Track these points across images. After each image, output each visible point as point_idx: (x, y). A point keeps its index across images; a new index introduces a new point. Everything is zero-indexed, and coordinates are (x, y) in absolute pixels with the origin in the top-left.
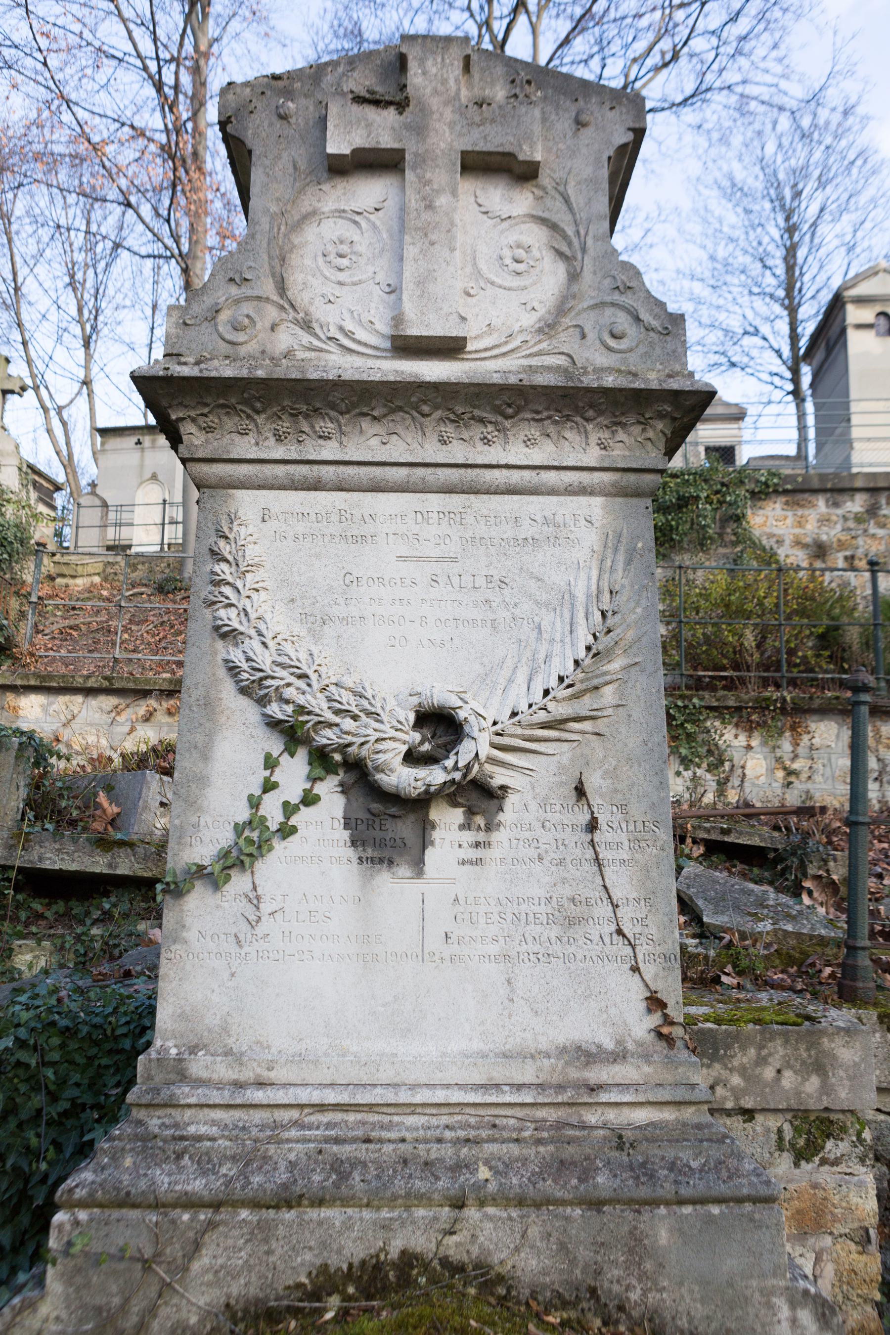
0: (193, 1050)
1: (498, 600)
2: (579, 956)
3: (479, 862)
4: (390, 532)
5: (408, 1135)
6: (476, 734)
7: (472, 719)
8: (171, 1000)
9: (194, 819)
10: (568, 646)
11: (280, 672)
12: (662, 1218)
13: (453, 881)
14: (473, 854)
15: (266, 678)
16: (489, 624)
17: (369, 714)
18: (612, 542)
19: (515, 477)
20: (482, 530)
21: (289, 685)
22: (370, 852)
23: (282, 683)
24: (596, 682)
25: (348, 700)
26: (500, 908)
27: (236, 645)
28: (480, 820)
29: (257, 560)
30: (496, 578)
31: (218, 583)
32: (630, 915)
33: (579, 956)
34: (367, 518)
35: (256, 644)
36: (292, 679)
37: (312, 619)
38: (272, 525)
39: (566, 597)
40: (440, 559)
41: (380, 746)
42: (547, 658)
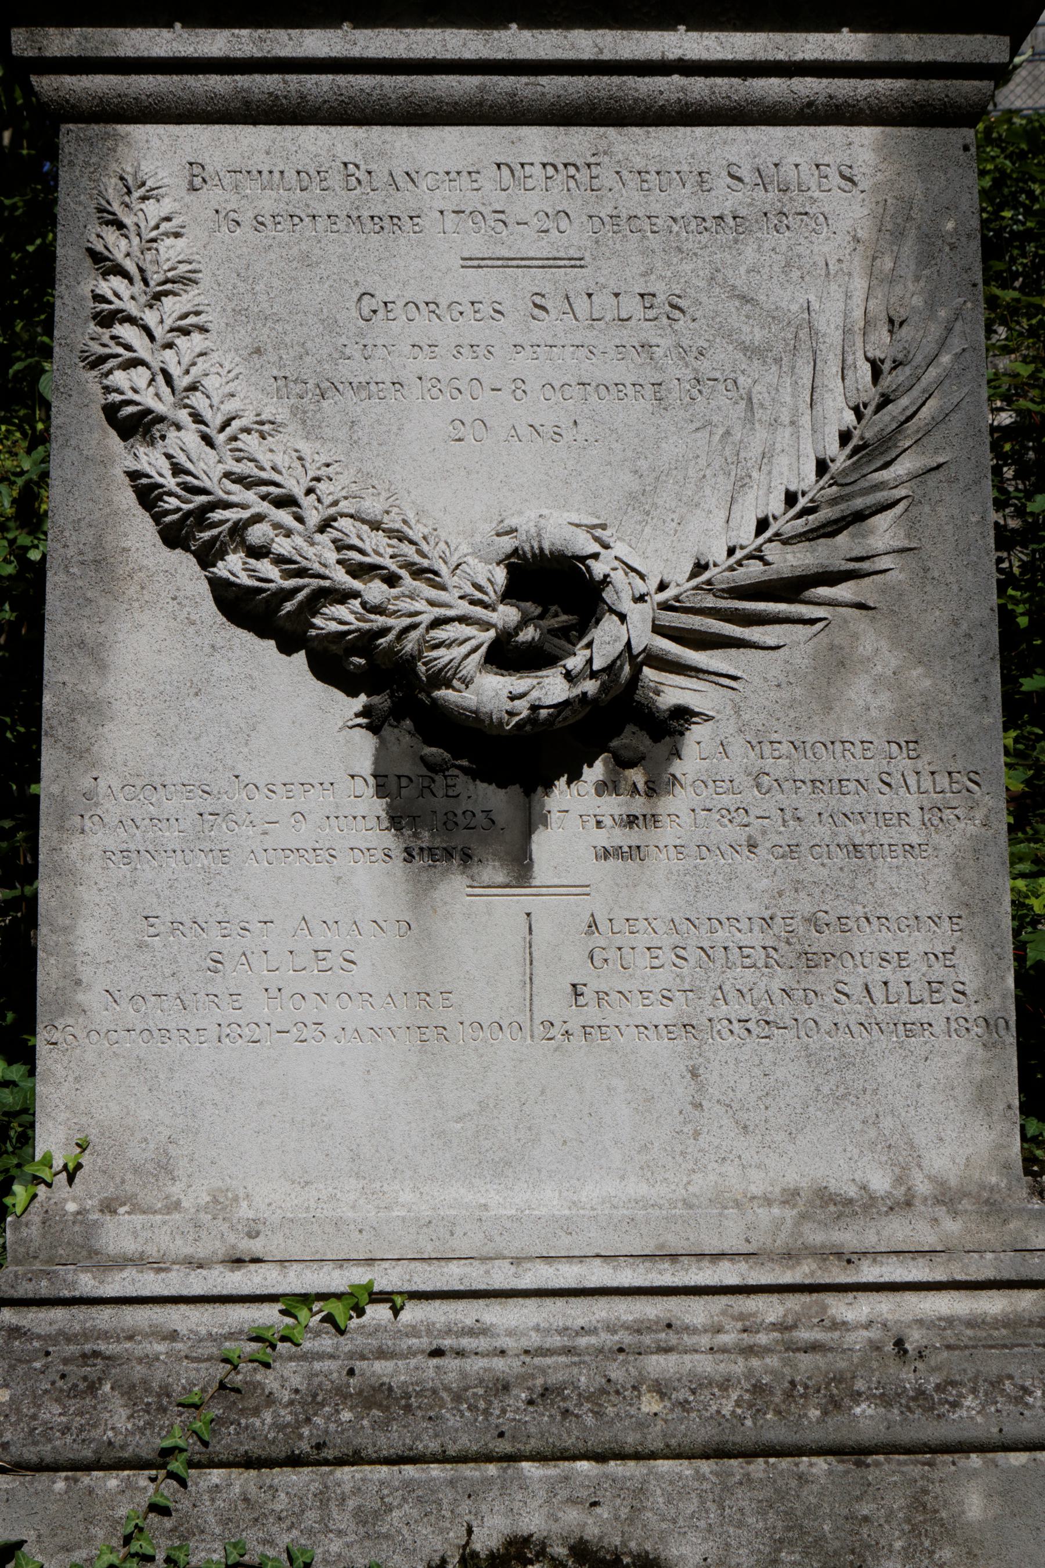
0: (109, 1207)
1: (666, 342)
2: (826, 1025)
3: (635, 852)
4: (449, 207)
5: (508, 1343)
6: (626, 605)
7: (618, 577)
8: (62, 1116)
9: (87, 783)
10: (806, 433)
11: (239, 494)
12: (974, 1473)
13: (583, 889)
14: (624, 838)
15: (213, 506)
16: (649, 391)
17: (419, 573)
18: (896, 223)
19: (700, 88)
20: (630, 200)
21: (258, 518)
22: (426, 838)
23: (245, 514)
24: (859, 503)
25: (378, 548)
26: (676, 939)
27: (152, 443)
28: (637, 776)
29: (183, 268)
30: (661, 298)
31: (107, 320)
32: (922, 948)
33: (826, 1025)
34: (402, 181)
35: (190, 437)
36: (265, 507)
37: (298, 388)
38: (213, 196)
39: (803, 334)
40: (551, 263)
41: (440, 634)
42: (766, 456)
